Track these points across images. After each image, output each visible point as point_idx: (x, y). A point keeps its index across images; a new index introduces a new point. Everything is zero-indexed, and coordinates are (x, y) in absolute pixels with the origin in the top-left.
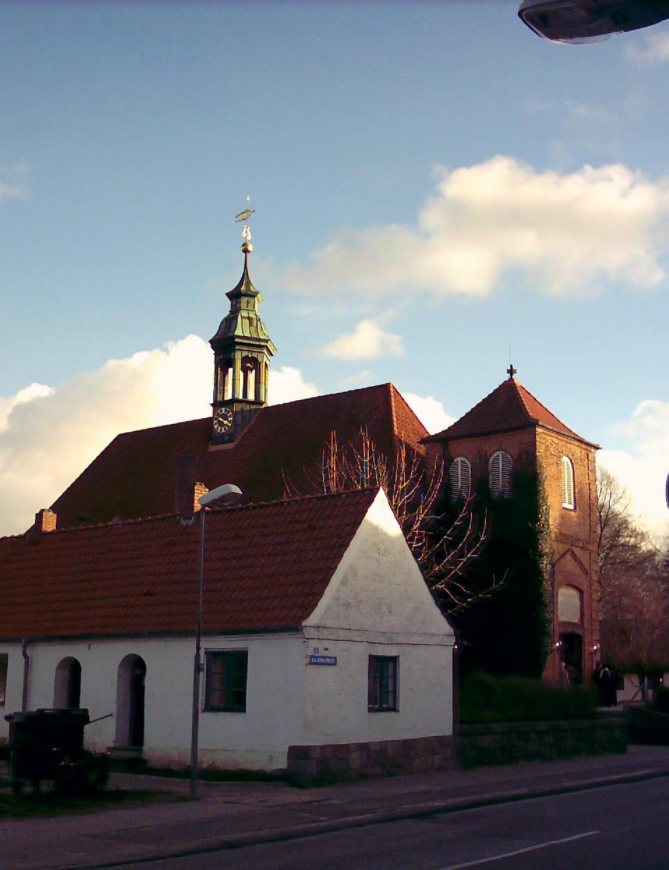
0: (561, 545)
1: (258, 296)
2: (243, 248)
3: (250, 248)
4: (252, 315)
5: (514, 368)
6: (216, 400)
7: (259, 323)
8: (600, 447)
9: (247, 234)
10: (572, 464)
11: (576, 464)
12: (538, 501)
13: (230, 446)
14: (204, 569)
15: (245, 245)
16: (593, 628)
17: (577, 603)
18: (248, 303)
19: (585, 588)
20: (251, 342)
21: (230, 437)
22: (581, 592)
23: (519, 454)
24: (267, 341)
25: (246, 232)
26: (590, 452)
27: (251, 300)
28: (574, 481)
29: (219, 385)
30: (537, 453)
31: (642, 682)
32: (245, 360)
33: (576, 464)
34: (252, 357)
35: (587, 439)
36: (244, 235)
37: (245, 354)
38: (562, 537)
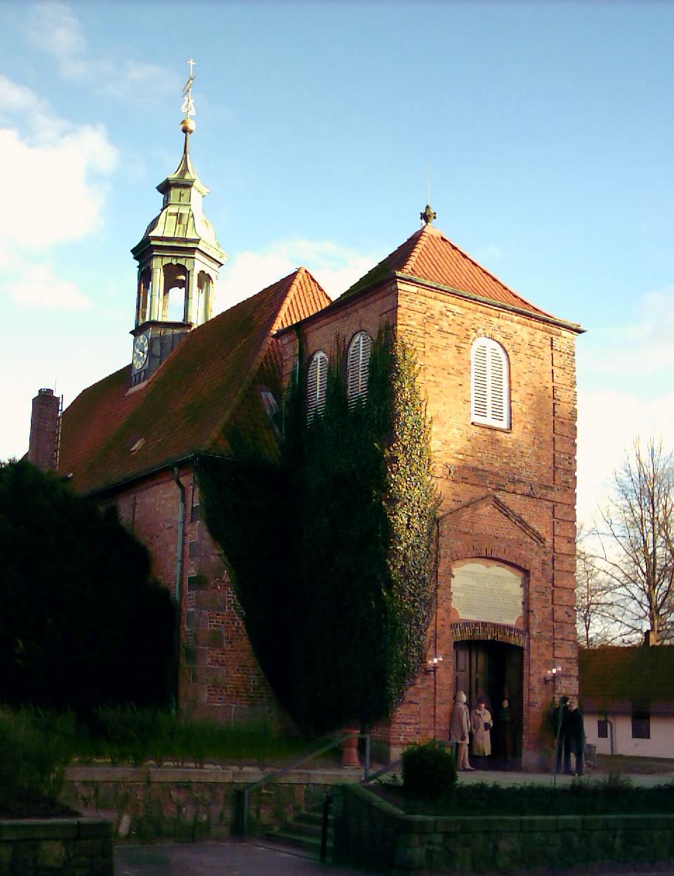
0: (462, 486)
1: (195, 184)
2: (182, 126)
3: (191, 125)
4: (184, 210)
5: (432, 211)
6: (138, 324)
7: (191, 219)
8: (582, 328)
9: (189, 108)
10: (506, 352)
11: (516, 353)
12: (393, 409)
13: (143, 384)
14: (177, 543)
15: (183, 122)
16: (558, 636)
17: (518, 591)
18: (181, 195)
19: (535, 564)
20: (175, 244)
21: (146, 372)
22: (526, 573)
23: (380, 332)
24: (197, 241)
25: (187, 106)
26: (559, 335)
27: (183, 191)
28: (510, 381)
29: (141, 304)
30: (399, 327)
31: (117, 830)
32: (168, 269)
33: (516, 353)
34: (178, 264)
35: (558, 316)
36: (184, 109)
37: (167, 261)
38: (466, 473)
